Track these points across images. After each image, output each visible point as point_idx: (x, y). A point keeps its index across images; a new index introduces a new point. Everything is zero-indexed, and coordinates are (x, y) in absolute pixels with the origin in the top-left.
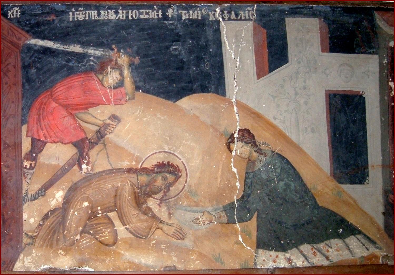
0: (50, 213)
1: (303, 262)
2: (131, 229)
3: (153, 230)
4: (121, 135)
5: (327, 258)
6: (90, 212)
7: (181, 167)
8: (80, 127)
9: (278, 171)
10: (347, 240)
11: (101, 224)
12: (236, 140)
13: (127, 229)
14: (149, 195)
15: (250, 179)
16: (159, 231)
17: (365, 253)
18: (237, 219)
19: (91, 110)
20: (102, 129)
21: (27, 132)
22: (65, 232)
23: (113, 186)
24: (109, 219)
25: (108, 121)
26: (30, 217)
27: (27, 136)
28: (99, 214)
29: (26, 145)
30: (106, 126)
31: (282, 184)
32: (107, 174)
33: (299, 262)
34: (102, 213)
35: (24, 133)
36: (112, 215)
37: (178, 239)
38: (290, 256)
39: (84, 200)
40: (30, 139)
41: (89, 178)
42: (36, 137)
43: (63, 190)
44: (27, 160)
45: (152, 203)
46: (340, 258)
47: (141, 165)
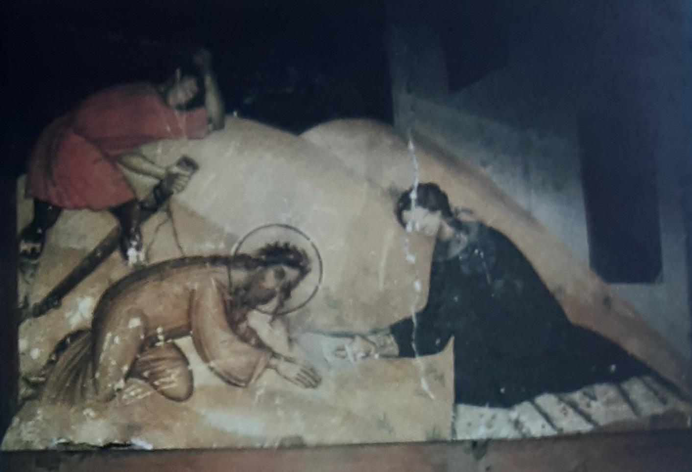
0: (68, 340)
1: (543, 427)
2: (219, 369)
3: (259, 370)
4: (197, 195)
5: (588, 418)
6: (142, 337)
7: (311, 253)
8: (125, 179)
9: (493, 259)
10: (626, 386)
11: (164, 359)
12: (413, 203)
13: (212, 369)
14: (251, 304)
15: (443, 271)
16: (270, 374)
17: (659, 409)
18: (418, 348)
19: (146, 150)
20: (165, 184)
21: (26, 191)
22: (97, 375)
23: (186, 289)
24: (178, 349)
25: (176, 170)
26: (33, 346)
27: (27, 196)
28: (159, 341)
29: (25, 212)
30: (172, 178)
31: (499, 283)
32: (174, 267)
33: (536, 427)
34: (166, 340)
35: (21, 190)
36: (185, 343)
37: (307, 387)
38: (519, 416)
39: (131, 314)
40: (30, 203)
41: (140, 274)
42: (42, 197)
43: (93, 295)
44: (26, 242)
45: (258, 320)
46: (611, 419)
47: (237, 249)
